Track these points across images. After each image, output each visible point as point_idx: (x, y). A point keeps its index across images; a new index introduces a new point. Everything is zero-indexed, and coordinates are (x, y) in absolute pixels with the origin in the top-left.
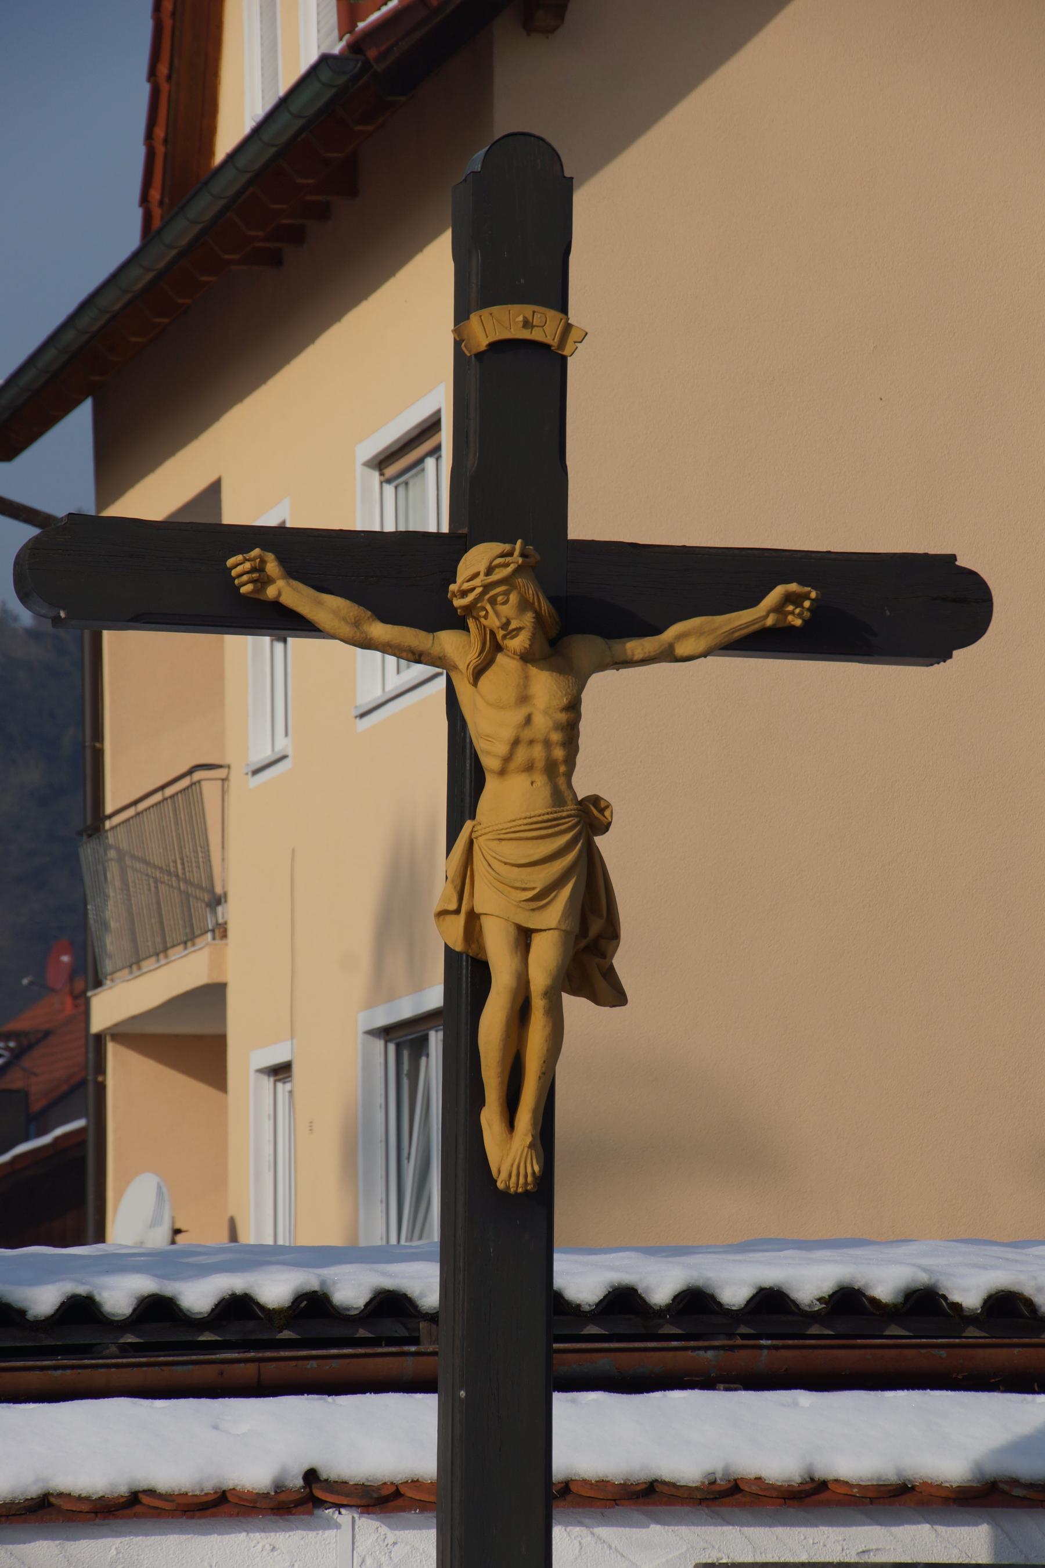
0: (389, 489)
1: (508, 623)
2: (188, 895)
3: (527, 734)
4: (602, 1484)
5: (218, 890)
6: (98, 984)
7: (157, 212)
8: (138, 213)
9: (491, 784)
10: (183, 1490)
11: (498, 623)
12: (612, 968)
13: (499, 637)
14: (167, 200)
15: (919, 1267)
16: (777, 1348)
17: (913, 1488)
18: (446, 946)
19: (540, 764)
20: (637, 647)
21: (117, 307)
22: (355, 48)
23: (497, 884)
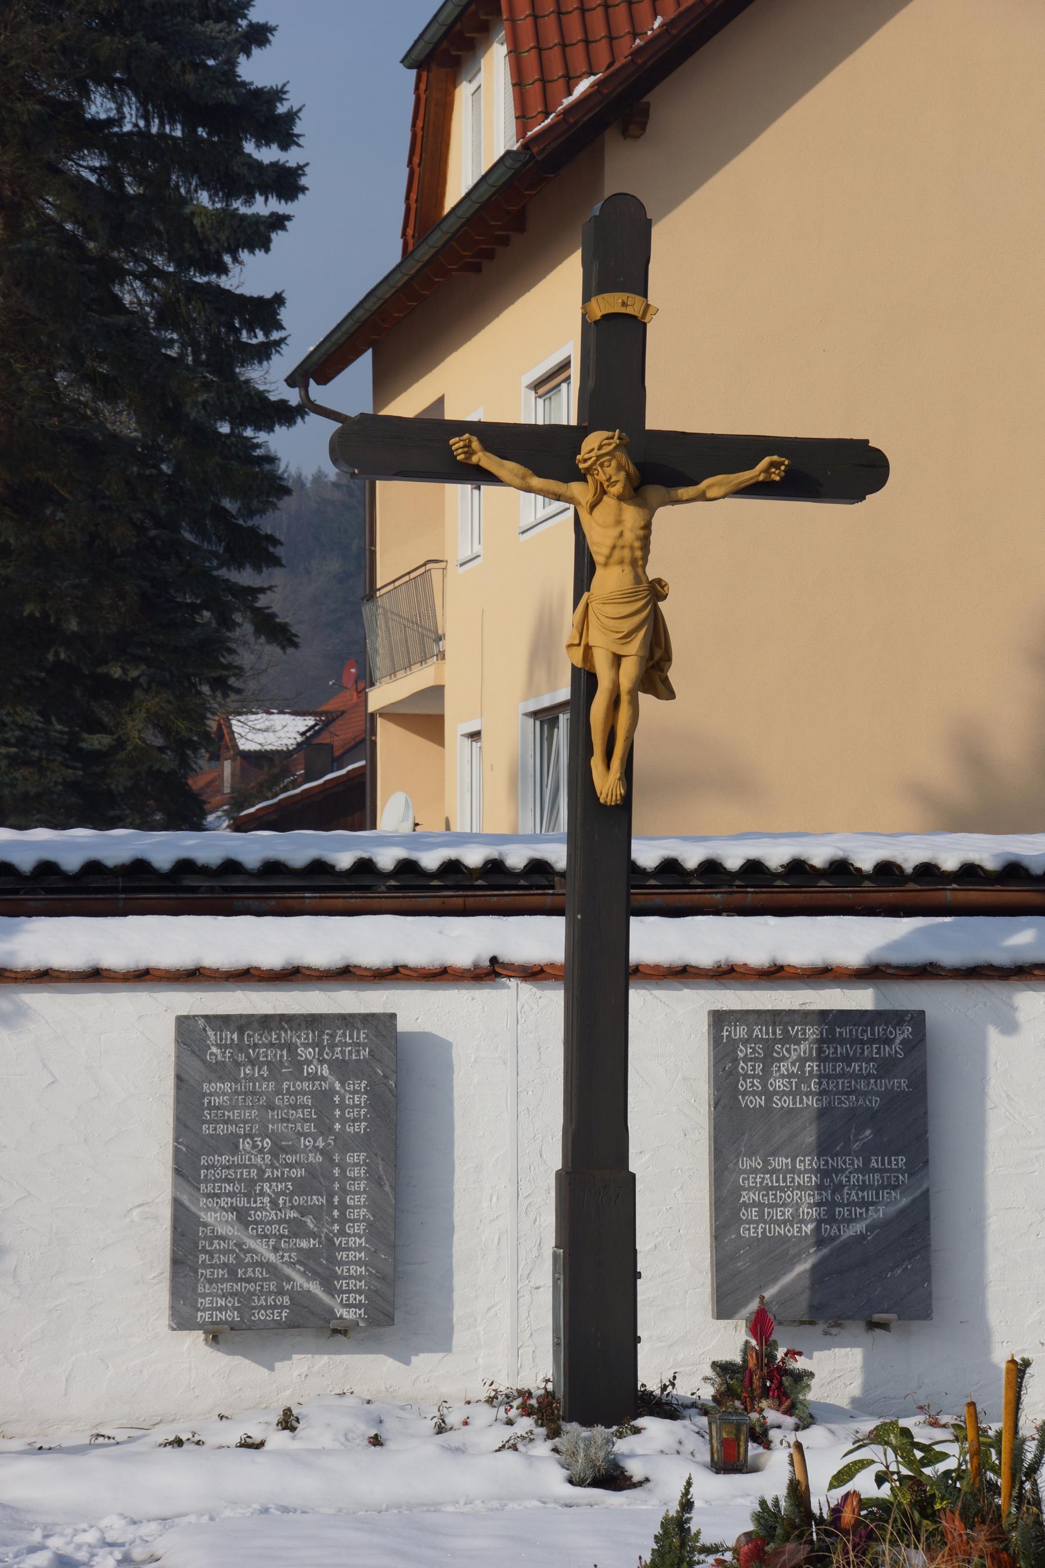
0: (540, 401)
1: (610, 478)
2: (423, 635)
3: (620, 543)
4: (657, 967)
5: (440, 632)
6: (372, 684)
7: (411, 241)
8: (401, 242)
9: (599, 572)
10: (423, 966)
11: (605, 478)
12: (667, 678)
13: (605, 486)
14: (416, 235)
15: (839, 848)
16: (757, 893)
17: (832, 969)
18: (572, 664)
19: (627, 560)
20: (684, 492)
21: (388, 296)
22: (526, 147)
23: (604, 630)
